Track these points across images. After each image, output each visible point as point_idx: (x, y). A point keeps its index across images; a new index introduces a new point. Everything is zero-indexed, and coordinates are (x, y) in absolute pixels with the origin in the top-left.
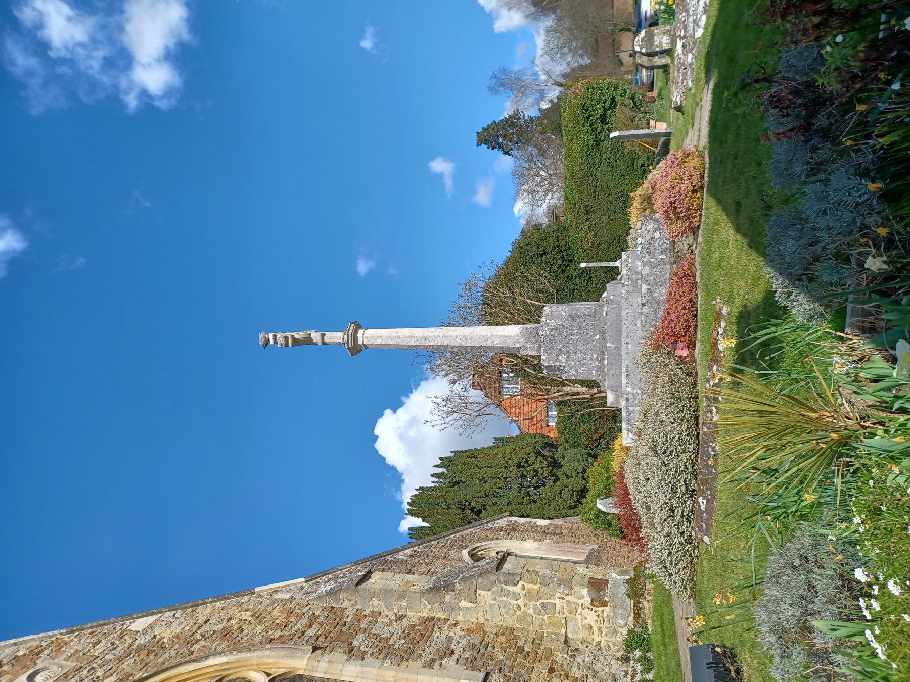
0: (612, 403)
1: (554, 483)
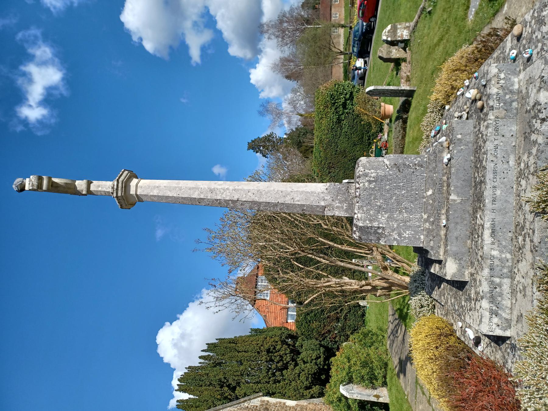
0: (454, 275)
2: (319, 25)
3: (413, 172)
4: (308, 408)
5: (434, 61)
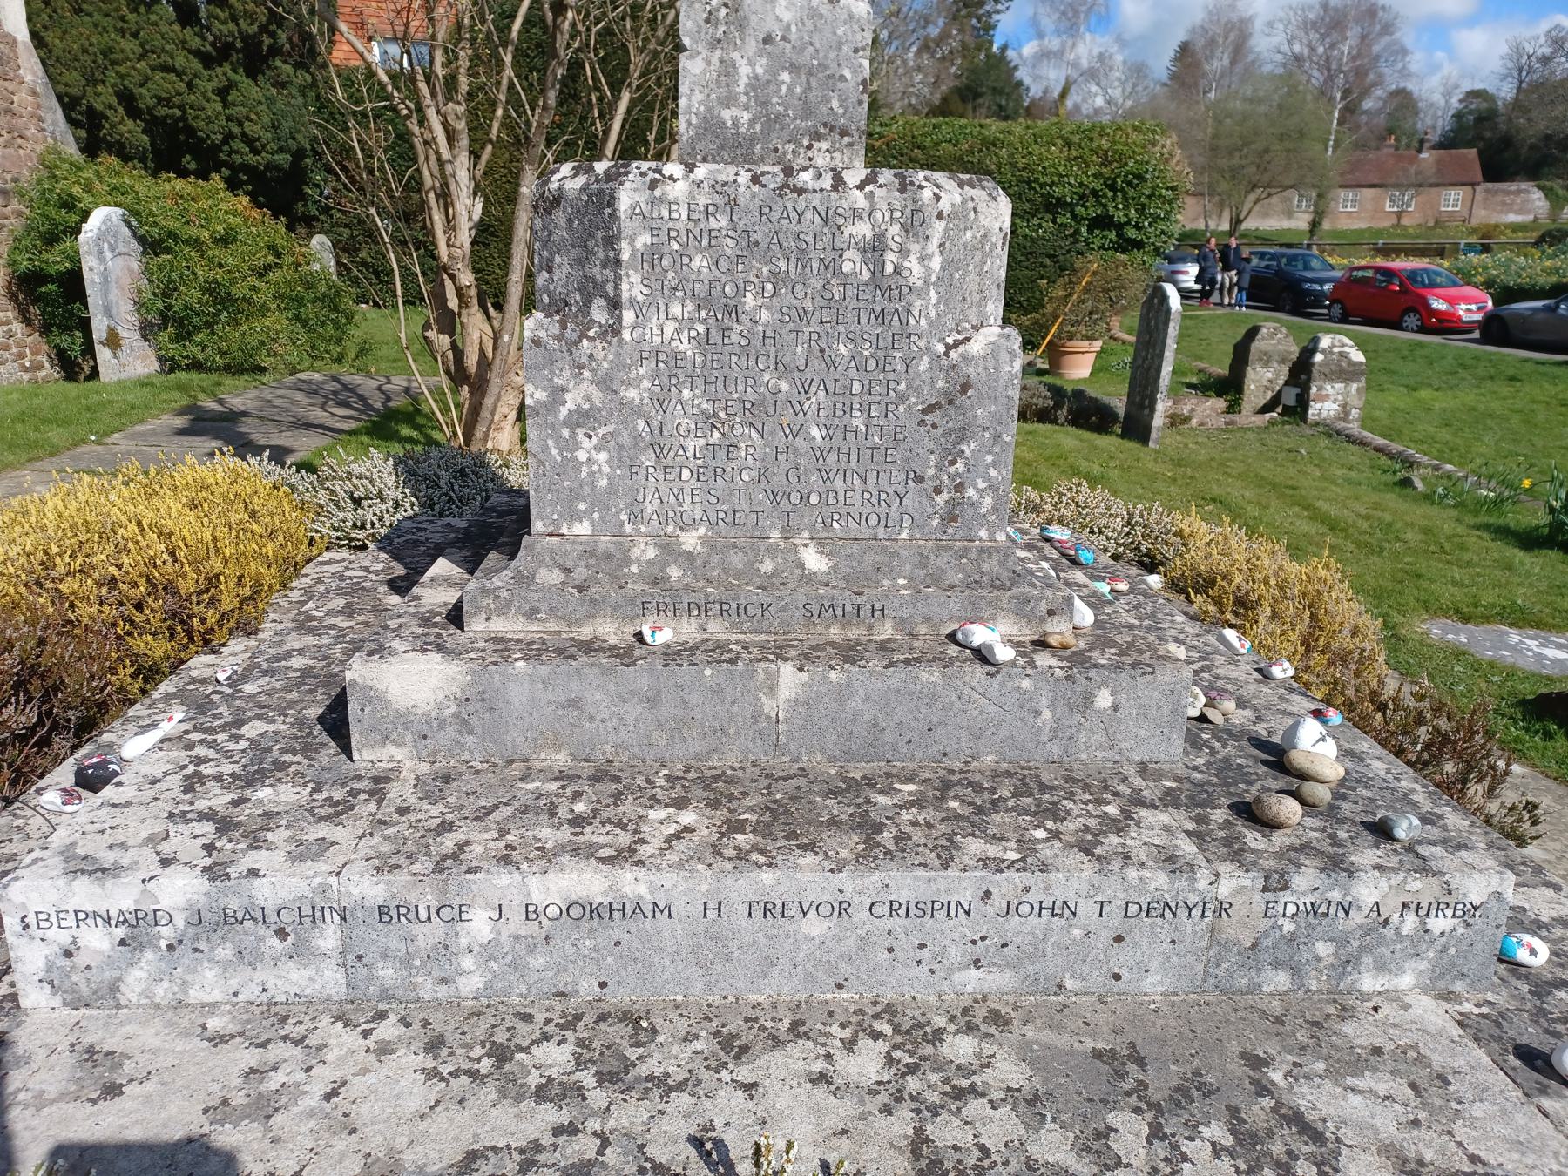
0: (374, 698)
1: (197, 53)
2: (1335, 148)
3: (919, 479)
4: (11, 86)
5: (1259, 503)
